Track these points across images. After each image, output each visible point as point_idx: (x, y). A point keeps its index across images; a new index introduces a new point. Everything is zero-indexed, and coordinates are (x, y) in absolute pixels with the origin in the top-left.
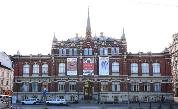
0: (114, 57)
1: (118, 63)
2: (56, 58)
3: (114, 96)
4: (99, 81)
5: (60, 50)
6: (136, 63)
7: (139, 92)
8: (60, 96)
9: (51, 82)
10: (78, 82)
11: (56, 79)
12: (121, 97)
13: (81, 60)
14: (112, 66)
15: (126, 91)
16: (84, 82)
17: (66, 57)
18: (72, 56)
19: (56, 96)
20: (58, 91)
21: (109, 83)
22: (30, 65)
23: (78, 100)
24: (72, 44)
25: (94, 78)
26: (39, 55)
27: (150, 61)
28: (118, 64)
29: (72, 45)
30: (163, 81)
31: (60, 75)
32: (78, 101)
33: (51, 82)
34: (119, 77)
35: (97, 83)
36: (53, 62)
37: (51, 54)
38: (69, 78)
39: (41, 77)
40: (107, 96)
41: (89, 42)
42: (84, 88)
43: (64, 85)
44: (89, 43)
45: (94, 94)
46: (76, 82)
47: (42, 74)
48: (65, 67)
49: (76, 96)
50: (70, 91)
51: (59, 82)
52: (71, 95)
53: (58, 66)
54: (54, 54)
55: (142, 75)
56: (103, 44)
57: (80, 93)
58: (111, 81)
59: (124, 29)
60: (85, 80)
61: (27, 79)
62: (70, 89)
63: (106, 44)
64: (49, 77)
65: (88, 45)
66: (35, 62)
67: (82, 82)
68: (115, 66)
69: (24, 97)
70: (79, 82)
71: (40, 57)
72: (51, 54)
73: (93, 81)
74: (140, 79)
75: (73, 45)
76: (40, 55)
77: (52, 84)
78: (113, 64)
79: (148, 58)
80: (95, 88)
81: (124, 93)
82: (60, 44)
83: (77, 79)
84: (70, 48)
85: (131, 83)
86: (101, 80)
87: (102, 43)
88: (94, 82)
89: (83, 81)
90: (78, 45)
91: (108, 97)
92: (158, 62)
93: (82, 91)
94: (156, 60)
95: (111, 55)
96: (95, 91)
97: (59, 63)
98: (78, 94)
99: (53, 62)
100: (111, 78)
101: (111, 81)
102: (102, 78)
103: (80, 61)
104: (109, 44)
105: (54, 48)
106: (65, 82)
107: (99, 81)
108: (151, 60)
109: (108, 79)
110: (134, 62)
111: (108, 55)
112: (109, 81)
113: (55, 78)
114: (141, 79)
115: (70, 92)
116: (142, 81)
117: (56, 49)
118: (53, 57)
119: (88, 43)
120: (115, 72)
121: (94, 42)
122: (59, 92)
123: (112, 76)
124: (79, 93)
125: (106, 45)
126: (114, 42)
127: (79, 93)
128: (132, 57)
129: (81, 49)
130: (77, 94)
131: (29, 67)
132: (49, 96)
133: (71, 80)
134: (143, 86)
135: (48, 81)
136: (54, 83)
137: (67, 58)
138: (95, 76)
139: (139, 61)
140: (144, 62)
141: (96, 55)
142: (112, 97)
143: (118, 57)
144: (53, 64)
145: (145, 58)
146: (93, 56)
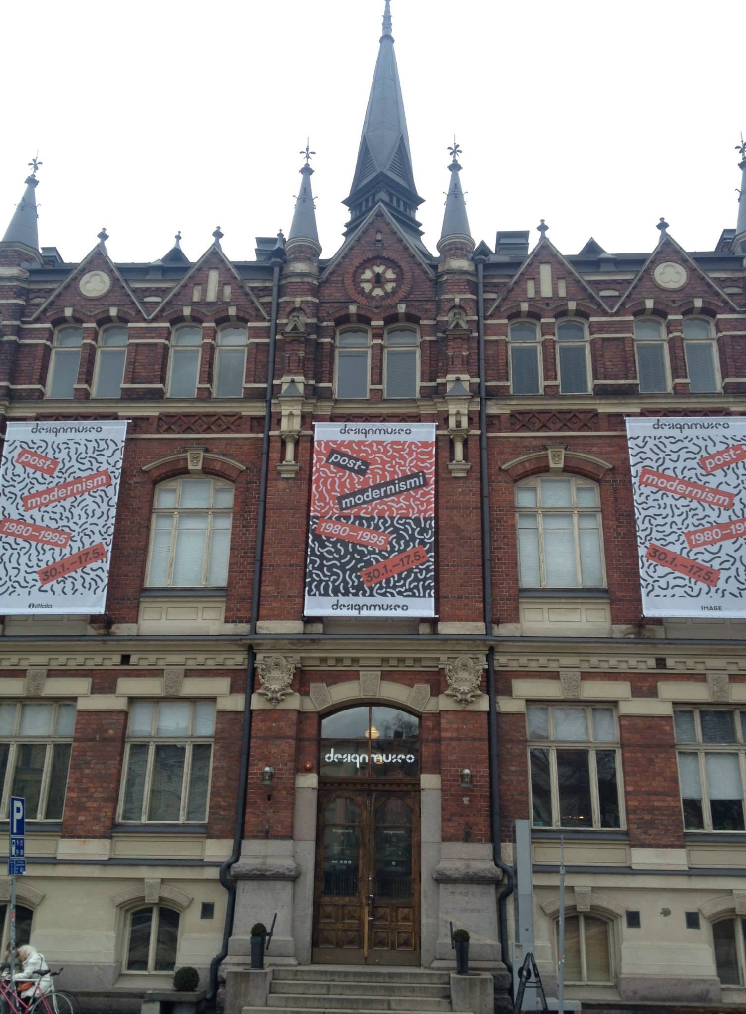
1: (221, 483)
3: (709, 907)
4: (508, 692)
5: (74, 343)
7: (631, 840)
10: (236, 703)
13: (290, 448)
16: (311, 705)
17: (605, 408)
18: (199, 399)
21: (629, 723)
23: (217, 963)
24: (204, 283)
29: (531, 285)
32: (217, 982)
38: (126, 659)
40: (619, 904)
41: (390, 263)
42: (309, 781)
44: (390, 275)
45: (442, 879)
46: (213, 699)
47: (144, 590)
49: (202, 895)
51: (132, 700)
52: (127, 893)
56: (204, 292)
59: (460, 159)
60: (333, 678)
65: (378, 292)
67: (294, 702)
70: (257, 703)
73: (427, 688)
75: (211, 297)
79: (540, 450)
80: (449, 795)
82: (76, 279)
83: (230, 664)
84: (177, 320)
85: (521, 715)
86: (524, 688)
88: (444, 703)
89: (305, 693)
90: (267, 291)
91: (634, 919)
92: (573, 464)
93: (289, 836)
95: (158, 396)
97: (155, 482)
100: (652, 663)
101: (653, 693)
102: (543, 660)
103: (275, 455)
107: (508, 692)
109: (612, 676)
110: (195, 466)
111: (129, 396)
115: (128, 848)
117: (19, 331)
119: (379, 280)
123: (524, 639)
124: (237, 852)
125: (569, 297)
126: (86, 278)
129: (302, 329)
130: (214, 873)
137: (618, 421)
138: (445, 628)
142: (692, 920)
143: (234, 422)
146: (426, 408)
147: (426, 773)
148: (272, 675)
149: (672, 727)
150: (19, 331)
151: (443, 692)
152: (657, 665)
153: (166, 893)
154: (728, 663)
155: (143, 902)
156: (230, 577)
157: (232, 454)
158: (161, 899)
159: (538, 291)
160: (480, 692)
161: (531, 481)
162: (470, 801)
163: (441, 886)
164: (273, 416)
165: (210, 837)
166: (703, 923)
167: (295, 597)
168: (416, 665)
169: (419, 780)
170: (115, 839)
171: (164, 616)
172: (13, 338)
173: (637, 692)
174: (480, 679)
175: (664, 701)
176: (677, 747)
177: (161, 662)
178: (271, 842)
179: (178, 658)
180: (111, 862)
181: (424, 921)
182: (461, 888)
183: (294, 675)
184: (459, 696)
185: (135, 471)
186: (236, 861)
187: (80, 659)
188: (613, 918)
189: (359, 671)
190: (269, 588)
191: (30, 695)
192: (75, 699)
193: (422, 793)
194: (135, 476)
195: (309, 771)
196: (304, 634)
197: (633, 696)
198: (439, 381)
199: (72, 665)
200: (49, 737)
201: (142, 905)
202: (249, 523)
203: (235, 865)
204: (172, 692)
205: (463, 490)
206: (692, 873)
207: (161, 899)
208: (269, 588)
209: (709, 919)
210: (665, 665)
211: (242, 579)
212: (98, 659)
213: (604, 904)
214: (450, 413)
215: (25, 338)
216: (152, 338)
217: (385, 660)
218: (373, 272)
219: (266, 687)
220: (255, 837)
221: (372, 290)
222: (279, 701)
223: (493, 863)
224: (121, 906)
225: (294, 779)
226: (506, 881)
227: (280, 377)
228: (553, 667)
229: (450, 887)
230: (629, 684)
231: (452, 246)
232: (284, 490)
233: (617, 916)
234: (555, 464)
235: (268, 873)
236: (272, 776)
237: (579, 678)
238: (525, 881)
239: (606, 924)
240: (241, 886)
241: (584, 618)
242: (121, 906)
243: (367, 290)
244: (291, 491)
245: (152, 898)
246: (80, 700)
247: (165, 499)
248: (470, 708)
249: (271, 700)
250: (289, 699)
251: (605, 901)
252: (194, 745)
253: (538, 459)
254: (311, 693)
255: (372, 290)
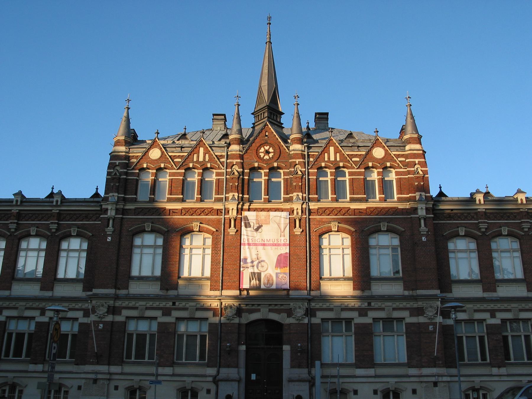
0: (143, 209)
2: (124, 212)
3: (380, 387)
6: (468, 239)
7: (492, 365)
8: (127, 389)
9: (93, 318)
11: (118, 303)
12: (414, 392)
13: (422, 222)
14: (372, 251)
15: (433, 364)
19: (113, 384)
20: (121, 363)
21: (38, 324)
22: (351, 235)
25: (292, 304)
26: (51, 195)
27: (481, 232)
28: (396, 242)
30: (411, 315)
31: (135, 289)
33: (93, 318)
34: (403, 298)
35: (304, 324)
36: (110, 229)
37: (102, 193)
39: (48, 294)
41: (271, 145)
43: (152, 336)
48: (160, 251)
49: (207, 386)
50: (128, 363)
51: (128, 318)
52: (180, 385)
53: (131, 246)
54: (116, 194)
55: (495, 291)
56: (198, 157)
57: (225, 372)
58: (366, 315)
59: (299, 101)
61: (30, 304)
62: (129, 356)
63: (342, 155)
64: (83, 295)
66: (506, 225)
68: (460, 255)
69: (7, 388)
71: (57, 206)
72: (102, 193)
74: (489, 308)
75: (332, 158)
76: (55, 200)
77: (97, 330)
78: (372, 242)
79: (472, 218)
80: (293, 352)
81: (426, 371)
86: (321, 315)
87: (323, 152)
88: (291, 320)
91: (356, 392)
93: (237, 366)
94: (461, 225)
96: (296, 364)
98: (216, 381)
99: (108, 226)
101: (366, 315)
103: (227, 225)
104: (356, 156)
105: (118, 168)
106: (155, 318)
107: (315, 316)
108: (483, 226)
112: (360, 315)
113: (111, 303)
114: (496, 308)
115: (179, 370)
116: (501, 315)
117: (126, 174)
118: (109, 207)
119: (267, 152)
120: (384, 275)
121: (291, 148)
122: (128, 369)
124: (218, 372)
125: (340, 161)
127: (221, 376)
128: (452, 210)
130: (211, 379)
131: (42, 250)
132: (79, 388)
133: (383, 309)
134: (505, 338)
135: (79, 314)
136: (104, 323)
139: (522, 229)
140: (499, 235)
141: (233, 198)
142: (375, 392)
144: (109, 235)
145: (502, 218)
147: (285, 345)
148: (297, 311)
149: (372, 327)
150: (126, 174)
151: (291, 316)
152: (368, 305)
153: (193, 386)
154: (508, 305)
155: (133, 387)
156: (211, 273)
157: (210, 224)
158: (192, 387)
159: (329, 158)
160: (236, 316)
161: (376, 235)
162: (300, 354)
163: (290, 383)
164: (226, 209)
165: (208, 367)
166: (379, 392)
167: (236, 281)
168: (282, 306)
169: (283, 347)
170: (174, 367)
171: (151, 287)
172: (125, 177)
173: (360, 315)
174: (305, 312)
175: (4, 316)
176: (127, 332)
177: (187, 305)
178: (230, 369)
179: (389, 304)
180: (173, 375)
181: (284, 395)
182: (297, 383)
183: (237, 311)
184: (297, 318)
185: (173, 231)
186: (218, 375)
187: (157, 303)
188: (349, 392)
189: (260, 309)
190: (226, 278)
191: (140, 316)
192: (78, 319)
193: (284, 352)
194: (173, 233)
195: (243, 344)
196: (320, 295)
197: (491, 318)
198: (291, 195)
199: (155, 305)
200: (147, 331)
201: (133, 388)
202: (218, 252)
203: (218, 377)
204: (192, 316)
205: (299, 240)
206: (376, 376)
207: (192, 387)
208: (226, 278)
209: (381, 391)
210: (371, 305)
211: (216, 274)
212: (164, 303)
213: (346, 388)
214: (230, 209)
215: (129, 176)
216: (178, 176)
217: (270, 305)
218: (264, 149)
219: (296, 315)
220: (225, 367)
221: (264, 156)
222: (102, 318)
223: (308, 375)
224: (178, 390)
225: (238, 347)
226: (312, 381)
227: (228, 193)
228: (509, 307)
229: (293, 383)
230: (489, 313)
231: (295, 139)
232: (231, 239)
233: (350, 391)
234: (384, 228)
235: (230, 379)
236: (230, 346)
237: (340, 310)
238: (318, 381)
239: (346, 394)
240: (220, 383)
241: (394, 288)
242: (178, 390)
243: (268, 158)
244: (233, 240)
245: (189, 387)
246: (36, 318)
247: (372, 242)
248: (301, 322)
249: (298, 320)
250: (235, 319)
251: (346, 386)
252: (201, 335)
253: (377, 226)
254: (243, 317)
255: (264, 156)
